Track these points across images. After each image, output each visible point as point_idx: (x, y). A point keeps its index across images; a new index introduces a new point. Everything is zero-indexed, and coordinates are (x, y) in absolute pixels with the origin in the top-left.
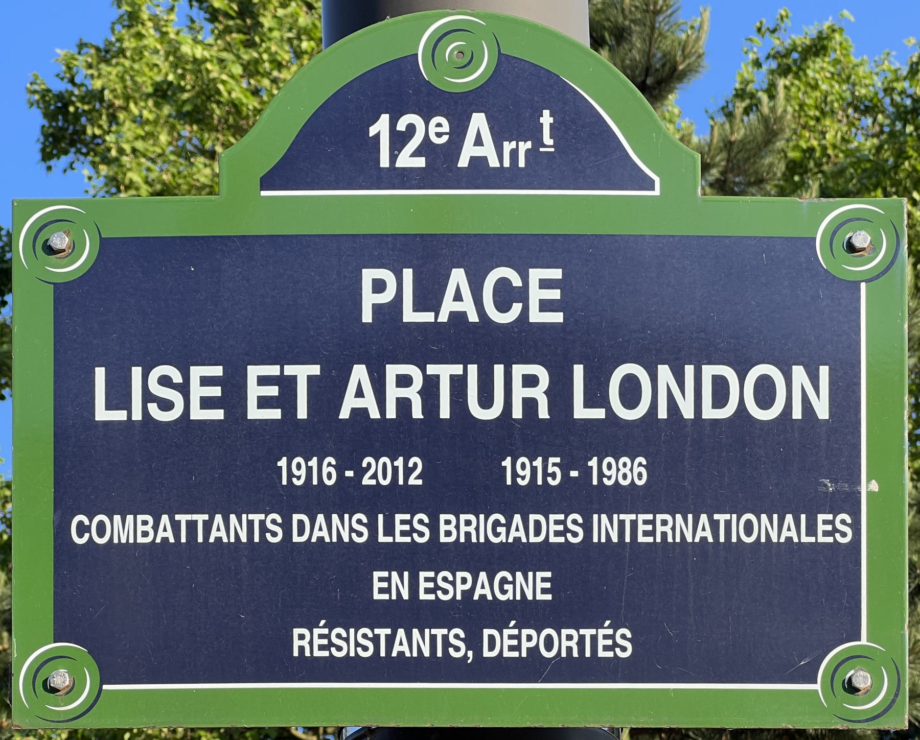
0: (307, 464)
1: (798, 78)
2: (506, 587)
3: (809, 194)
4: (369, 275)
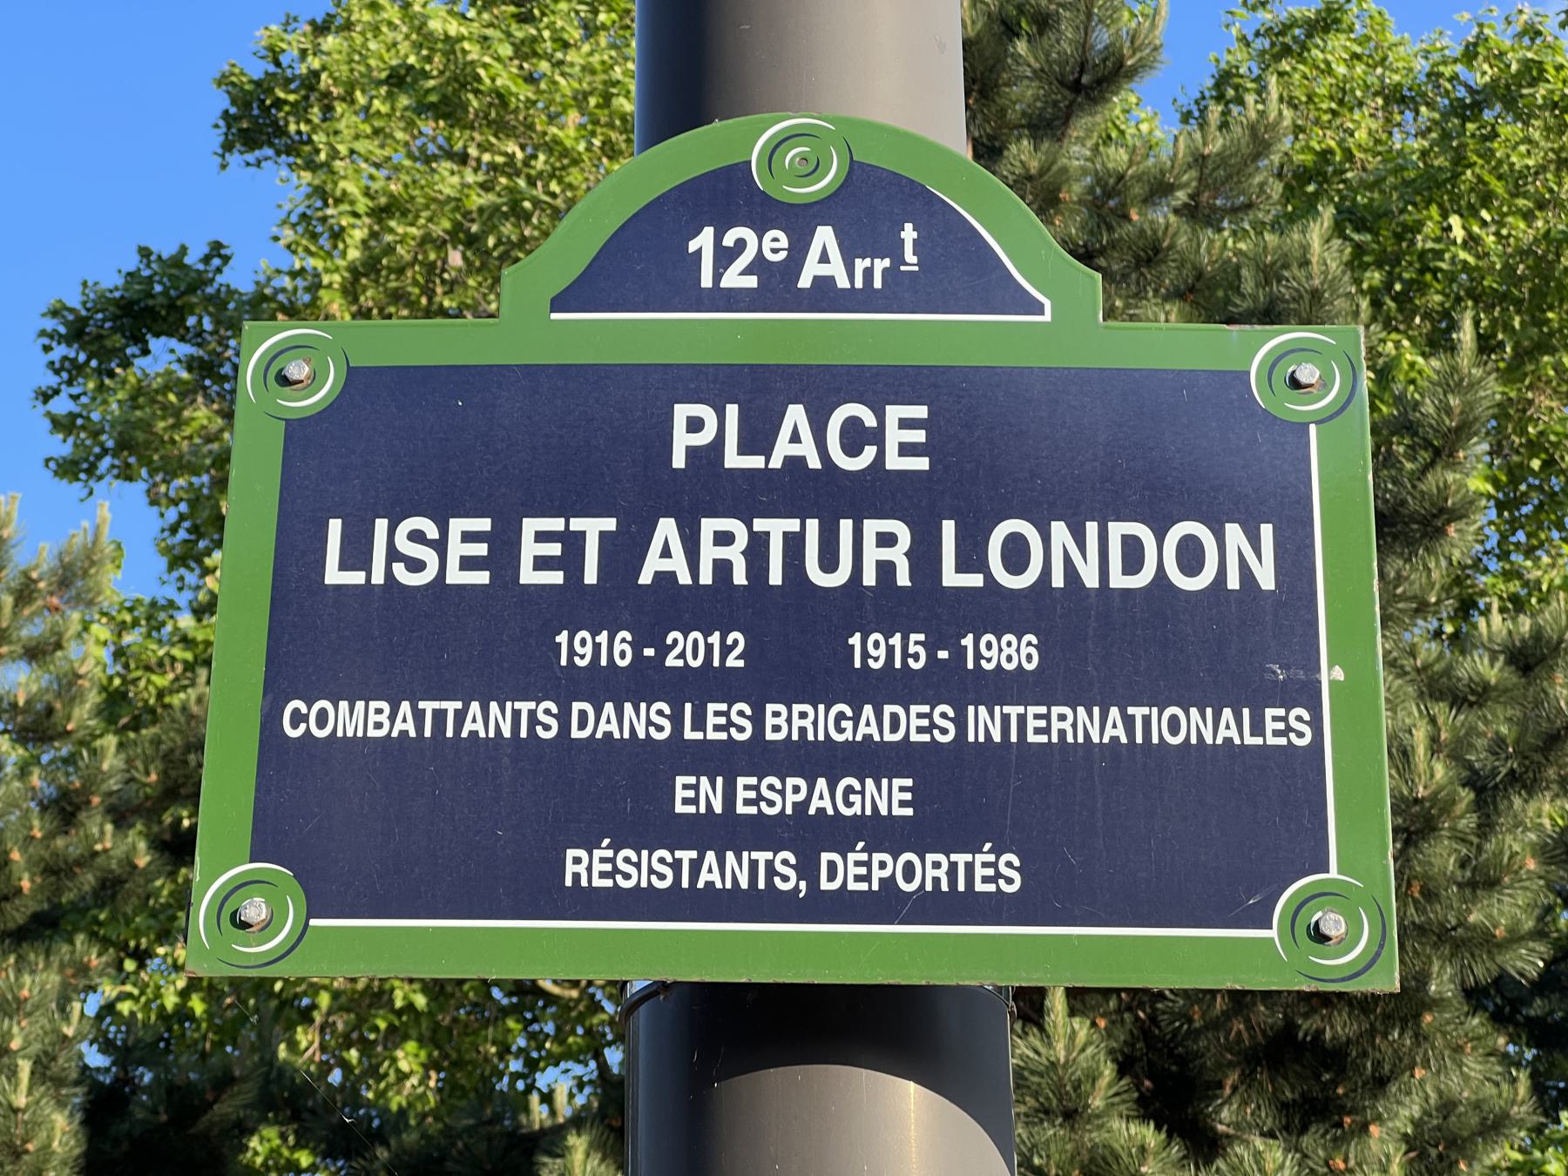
0: (594, 639)
1: (1303, 61)
2: (852, 798)
3: (1318, 224)
4: (682, 412)
